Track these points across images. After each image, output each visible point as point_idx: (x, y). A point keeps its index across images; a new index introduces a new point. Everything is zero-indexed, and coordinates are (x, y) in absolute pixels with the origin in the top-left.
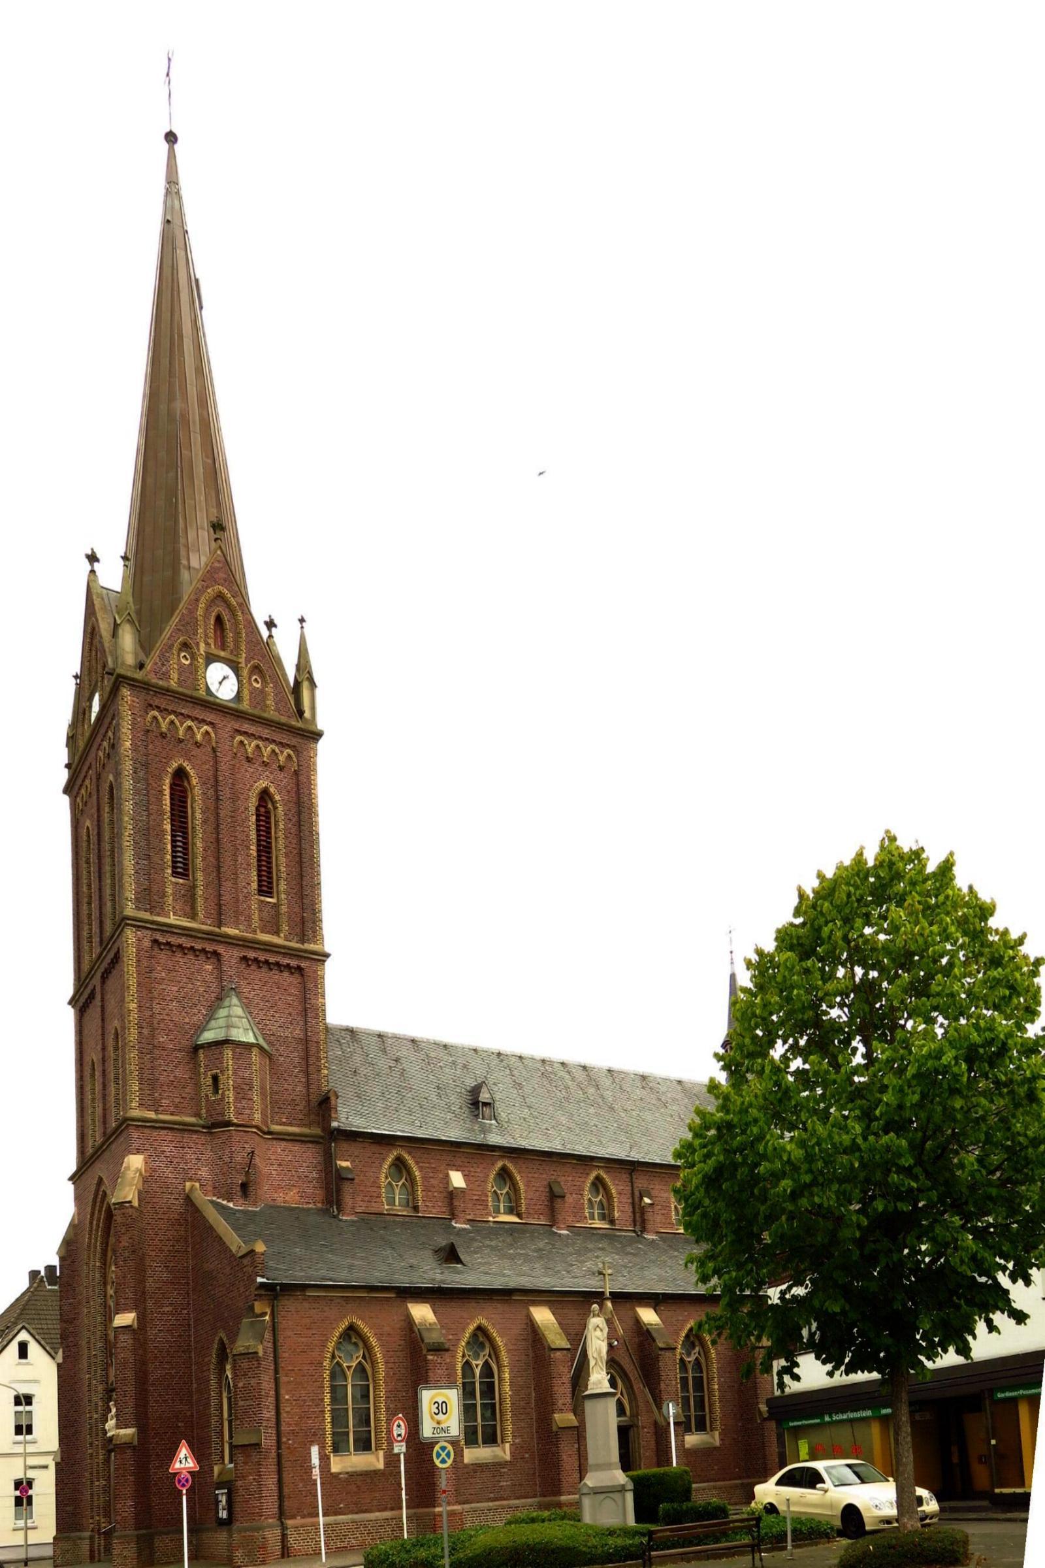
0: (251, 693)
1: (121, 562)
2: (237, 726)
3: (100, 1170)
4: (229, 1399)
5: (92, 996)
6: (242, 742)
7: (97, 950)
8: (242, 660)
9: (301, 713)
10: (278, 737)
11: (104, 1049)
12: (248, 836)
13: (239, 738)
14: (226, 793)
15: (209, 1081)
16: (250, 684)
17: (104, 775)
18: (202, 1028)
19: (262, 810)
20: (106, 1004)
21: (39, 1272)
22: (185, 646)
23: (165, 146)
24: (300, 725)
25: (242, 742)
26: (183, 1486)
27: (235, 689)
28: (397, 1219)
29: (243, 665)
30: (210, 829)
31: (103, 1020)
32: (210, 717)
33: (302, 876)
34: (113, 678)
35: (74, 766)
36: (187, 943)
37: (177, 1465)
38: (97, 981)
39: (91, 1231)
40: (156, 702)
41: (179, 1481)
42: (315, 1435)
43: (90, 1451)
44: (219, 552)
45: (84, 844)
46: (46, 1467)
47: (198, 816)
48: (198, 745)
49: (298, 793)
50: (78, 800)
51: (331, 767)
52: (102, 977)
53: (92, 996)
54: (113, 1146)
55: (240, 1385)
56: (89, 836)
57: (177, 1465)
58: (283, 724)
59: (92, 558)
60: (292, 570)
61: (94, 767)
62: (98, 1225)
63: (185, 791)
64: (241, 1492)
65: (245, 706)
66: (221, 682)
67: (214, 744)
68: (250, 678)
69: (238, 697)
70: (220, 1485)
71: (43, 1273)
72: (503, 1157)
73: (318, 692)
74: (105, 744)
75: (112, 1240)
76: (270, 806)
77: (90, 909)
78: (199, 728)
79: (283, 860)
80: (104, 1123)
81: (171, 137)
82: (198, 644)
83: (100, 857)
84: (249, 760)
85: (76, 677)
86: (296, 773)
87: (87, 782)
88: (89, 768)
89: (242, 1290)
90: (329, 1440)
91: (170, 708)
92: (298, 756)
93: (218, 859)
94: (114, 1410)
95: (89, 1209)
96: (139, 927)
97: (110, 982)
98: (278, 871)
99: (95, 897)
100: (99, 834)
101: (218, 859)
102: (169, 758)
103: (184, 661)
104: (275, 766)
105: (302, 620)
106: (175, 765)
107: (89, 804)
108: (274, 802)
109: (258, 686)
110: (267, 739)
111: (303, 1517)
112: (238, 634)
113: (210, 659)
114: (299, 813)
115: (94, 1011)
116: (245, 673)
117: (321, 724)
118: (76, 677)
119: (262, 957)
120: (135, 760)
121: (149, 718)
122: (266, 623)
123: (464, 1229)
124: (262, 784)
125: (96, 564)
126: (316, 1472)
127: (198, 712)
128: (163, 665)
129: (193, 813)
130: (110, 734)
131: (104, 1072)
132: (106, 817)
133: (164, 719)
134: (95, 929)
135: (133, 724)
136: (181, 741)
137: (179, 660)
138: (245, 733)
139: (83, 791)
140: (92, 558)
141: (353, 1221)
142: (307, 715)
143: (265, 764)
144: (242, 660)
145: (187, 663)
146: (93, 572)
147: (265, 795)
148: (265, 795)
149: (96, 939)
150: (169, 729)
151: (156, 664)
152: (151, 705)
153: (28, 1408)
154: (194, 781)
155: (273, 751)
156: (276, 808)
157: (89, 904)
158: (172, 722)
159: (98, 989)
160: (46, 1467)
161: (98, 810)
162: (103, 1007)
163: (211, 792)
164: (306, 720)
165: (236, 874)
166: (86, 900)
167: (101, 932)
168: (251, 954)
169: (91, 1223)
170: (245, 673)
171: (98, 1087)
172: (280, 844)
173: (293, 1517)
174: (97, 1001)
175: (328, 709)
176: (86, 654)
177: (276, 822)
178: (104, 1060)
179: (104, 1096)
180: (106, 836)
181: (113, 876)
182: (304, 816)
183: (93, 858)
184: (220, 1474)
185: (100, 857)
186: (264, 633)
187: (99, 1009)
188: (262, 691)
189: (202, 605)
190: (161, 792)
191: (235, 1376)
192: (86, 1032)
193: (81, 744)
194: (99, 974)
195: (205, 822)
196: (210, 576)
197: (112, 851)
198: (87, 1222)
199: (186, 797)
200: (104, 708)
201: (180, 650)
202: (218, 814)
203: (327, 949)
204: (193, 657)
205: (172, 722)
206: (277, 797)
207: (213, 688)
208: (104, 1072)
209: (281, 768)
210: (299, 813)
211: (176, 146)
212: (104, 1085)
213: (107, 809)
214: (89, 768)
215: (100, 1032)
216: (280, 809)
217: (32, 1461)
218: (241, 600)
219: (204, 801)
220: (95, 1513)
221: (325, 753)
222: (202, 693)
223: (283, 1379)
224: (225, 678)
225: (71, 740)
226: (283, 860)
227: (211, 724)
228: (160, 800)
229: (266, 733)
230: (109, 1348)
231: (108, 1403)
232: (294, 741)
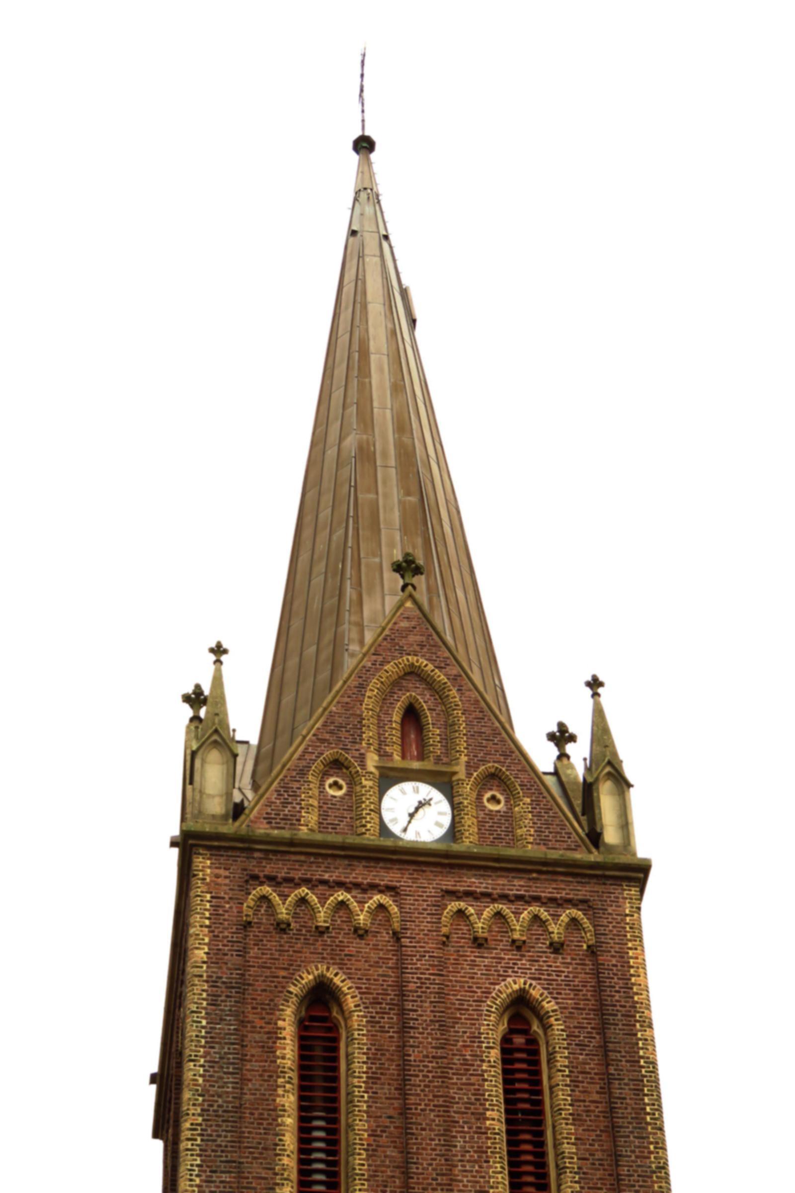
0: (481, 824)
2: (448, 883)
6: (460, 913)
8: (461, 769)
9: (595, 837)
10: (547, 890)
12: (479, 1094)
13: (454, 906)
14: (423, 1013)
16: (480, 806)
19: (519, 1040)
22: (337, 765)
24: (594, 857)
25: (460, 913)
27: (446, 821)
29: (462, 775)
30: (386, 1090)
32: (387, 877)
33: (616, 1157)
40: (269, 869)
44: (409, 604)
47: (360, 1065)
48: (360, 933)
49: (599, 988)
51: (687, 960)
58: (556, 863)
63: (335, 1028)
65: (469, 843)
66: (416, 814)
67: (396, 926)
68: (479, 797)
69: (454, 833)
73: (634, 795)
76: (536, 1027)
78: (361, 903)
79: (567, 1129)
82: (362, 758)
84: (479, 943)
86: (592, 951)
91: (297, 875)
92: (593, 919)
93: (405, 1151)
96: (219, 848)
98: (559, 1155)
101: (405, 1151)
102: (292, 969)
103: (331, 792)
104: (542, 946)
105: (595, 684)
106: (308, 978)
108: (543, 1018)
109: (500, 807)
110: (520, 898)
112: (449, 726)
113: (390, 778)
114: (603, 1028)
116: (467, 789)
117: (644, 847)
120: (213, 982)
121: (251, 901)
124: (513, 984)
126: (520, 1128)
127: (360, 874)
128: (285, 804)
129: (349, 1063)
133: (284, 897)
135: (215, 914)
136: (321, 932)
137: (322, 791)
138: (469, 895)
142: (611, 836)
143: (518, 946)
144: (461, 769)
145: (339, 793)
147: (521, 1008)
148: (521, 1008)
150: (296, 915)
151: (270, 804)
152: (255, 877)
154: (350, 1003)
155: (536, 918)
156: (546, 1027)
158: (303, 901)
163: (390, 1020)
164: (610, 849)
165: (449, 1173)
170: (467, 789)
172: (560, 1095)
175: (653, 825)
177: (551, 1061)
182: (615, 1033)
188: (508, 816)
189: (372, 691)
190: (274, 1035)
195: (373, 1079)
196: (391, 642)
199: (336, 1040)
201: (325, 774)
202: (404, 1056)
204: (353, 781)
206: (549, 1005)
207: (396, 829)
209: (557, 948)
210: (603, 1028)
216: (558, 1027)
218: (455, 670)
219: (371, 1036)
222: (371, 837)
224: (421, 805)
226: (567, 1129)
227: (390, 889)
228: (269, 1050)
229: (517, 886)
232: (582, 891)
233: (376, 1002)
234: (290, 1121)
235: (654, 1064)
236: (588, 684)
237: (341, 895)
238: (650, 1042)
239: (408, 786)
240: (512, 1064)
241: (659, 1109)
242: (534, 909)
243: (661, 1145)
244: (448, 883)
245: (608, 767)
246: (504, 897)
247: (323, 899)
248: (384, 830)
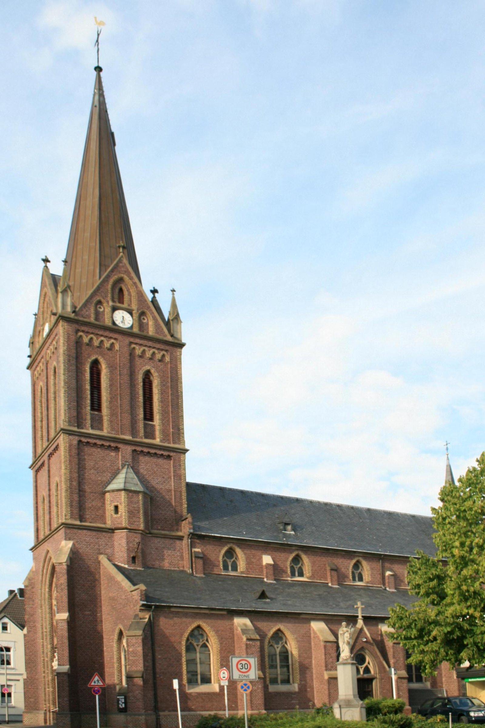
1: (63, 263)
3: (46, 546)
4: (125, 656)
5: (43, 465)
7: (45, 444)
10: (158, 346)
11: (50, 490)
15: (112, 508)
17: (50, 362)
18: (109, 483)
19: (147, 380)
20: (51, 469)
21: (14, 591)
23: (95, 73)
26: (96, 693)
28: (230, 577)
31: (49, 477)
34: (56, 317)
35: (33, 357)
36: (99, 442)
37: (93, 684)
38: (46, 457)
39: (43, 575)
41: (94, 691)
42: (176, 674)
43: (43, 675)
45: (39, 394)
46: (18, 680)
50: (36, 372)
51: (190, 363)
52: (49, 456)
53: (43, 465)
54: (55, 536)
55: (131, 650)
56: (41, 390)
57: (93, 684)
59: (46, 260)
60: (164, 255)
61: (45, 358)
62: (47, 572)
64: (132, 698)
65: (136, 330)
66: (124, 319)
70: (120, 694)
71: (16, 592)
72: (297, 550)
74: (51, 347)
75: (55, 580)
77: (42, 424)
80: (50, 525)
81: (99, 69)
83: (47, 400)
85: (35, 315)
87: (41, 364)
88: (42, 358)
89: (132, 606)
90: (185, 677)
91: (91, 331)
94: (57, 658)
95: (42, 565)
97: (53, 459)
99: (45, 419)
100: (47, 389)
105: (173, 291)
106: (93, 358)
107: (42, 375)
111: (169, 711)
113: (114, 309)
115: (44, 472)
118: (35, 315)
119: (146, 450)
122: (152, 291)
123: (271, 584)
124: (147, 367)
125: (48, 264)
127: (107, 333)
130: (54, 343)
131: (50, 502)
132: (51, 382)
134: (45, 434)
139: (38, 368)
140: (46, 260)
141: (202, 577)
146: (46, 266)
148: (148, 374)
149: (45, 439)
153: (8, 653)
157: (42, 421)
159: (46, 462)
160: (18, 680)
161: (47, 378)
162: (49, 471)
166: (40, 419)
167: (48, 435)
168: (139, 449)
169: (43, 571)
171: (47, 508)
173: (164, 711)
174: (46, 467)
175: (186, 332)
176: (41, 304)
178: (49, 496)
179: (50, 513)
180: (52, 390)
181: (55, 410)
183: (44, 400)
184: (120, 690)
185: (47, 400)
186: (150, 296)
187: (47, 472)
191: (128, 646)
192: (39, 482)
193: (38, 346)
194: (47, 455)
197: (55, 398)
198: (41, 570)
200: (51, 330)
203: (187, 447)
205: (91, 339)
208: (50, 502)
211: (101, 74)
212: (50, 507)
213: (52, 377)
214: (42, 358)
215: (47, 482)
217: (9, 677)
220: (47, 703)
221: (186, 356)
223: (157, 649)
225: (32, 343)
227: (115, 339)
229: (150, 343)
230: (53, 629)
231: (53, 654)
232: (167, 348)
233: (112, 367)
234: (89, 392)
235: (182, 392)
236: (172, 291)
237: (102, 338)
238: (181, 387)
239: (121, 311)
240: (175, 690)
241: (182, 403)
242: (154, 350)
243: (182, 411)
244: (132, 340)
245: (176, 318)
246: (146, 346)
247: (97, 339)
248: (114, 323)
